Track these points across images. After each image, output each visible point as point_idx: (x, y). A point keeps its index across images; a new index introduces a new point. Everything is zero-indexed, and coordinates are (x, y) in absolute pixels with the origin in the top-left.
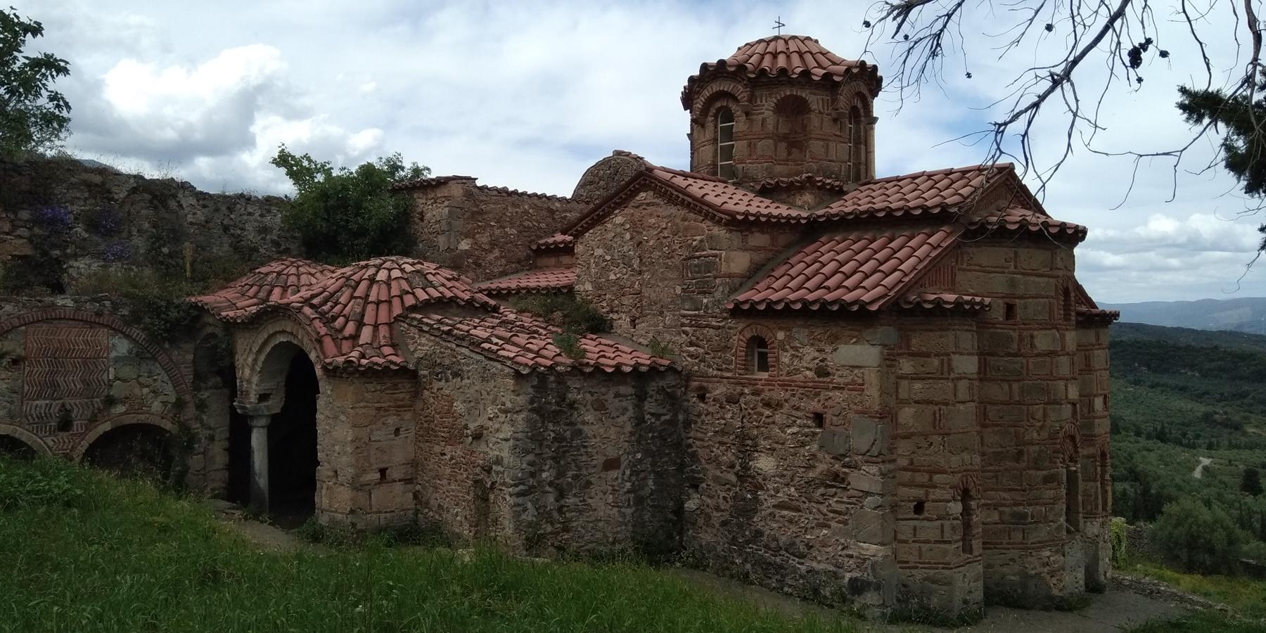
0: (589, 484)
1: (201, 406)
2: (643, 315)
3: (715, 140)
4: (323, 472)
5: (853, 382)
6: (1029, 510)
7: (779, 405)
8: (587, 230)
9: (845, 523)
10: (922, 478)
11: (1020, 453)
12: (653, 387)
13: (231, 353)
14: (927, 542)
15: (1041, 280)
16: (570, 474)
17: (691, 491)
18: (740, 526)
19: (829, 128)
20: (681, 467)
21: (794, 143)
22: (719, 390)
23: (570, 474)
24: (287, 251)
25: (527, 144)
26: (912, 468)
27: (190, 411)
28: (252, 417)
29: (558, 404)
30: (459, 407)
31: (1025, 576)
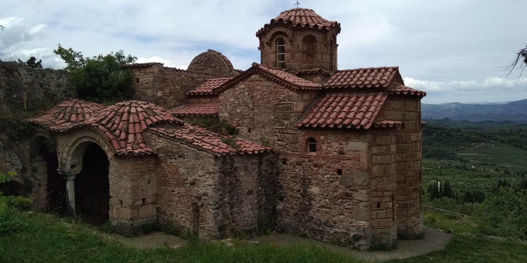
0: (242, 201)
1: (34, 170)
2: (254, 127)
3: (276, 52)
4: (114, 201)
5: (355, 157)
6: (408, 202)
7: (321, 166)
8: (225, 90)
9: (351, 213)
10: (380, 194)
11: (406, 181)
12: (264, 159)
13: (55, 146)
14: (381, 218)
15: (413, 113)
16: (235, 198)
17: (279, 201)
18: (303, 215)
19: (324, 49)
20: (275, 192)
21: (310, 54)
22: (293, 160)
23: (235, 198)
24: (70, 95)
25: (117, 35)
26: (376, 190)
27: (29, 173)
28: (67, 176)
29: (231, 169)
30: (182, 170)
31: (407, 227)
